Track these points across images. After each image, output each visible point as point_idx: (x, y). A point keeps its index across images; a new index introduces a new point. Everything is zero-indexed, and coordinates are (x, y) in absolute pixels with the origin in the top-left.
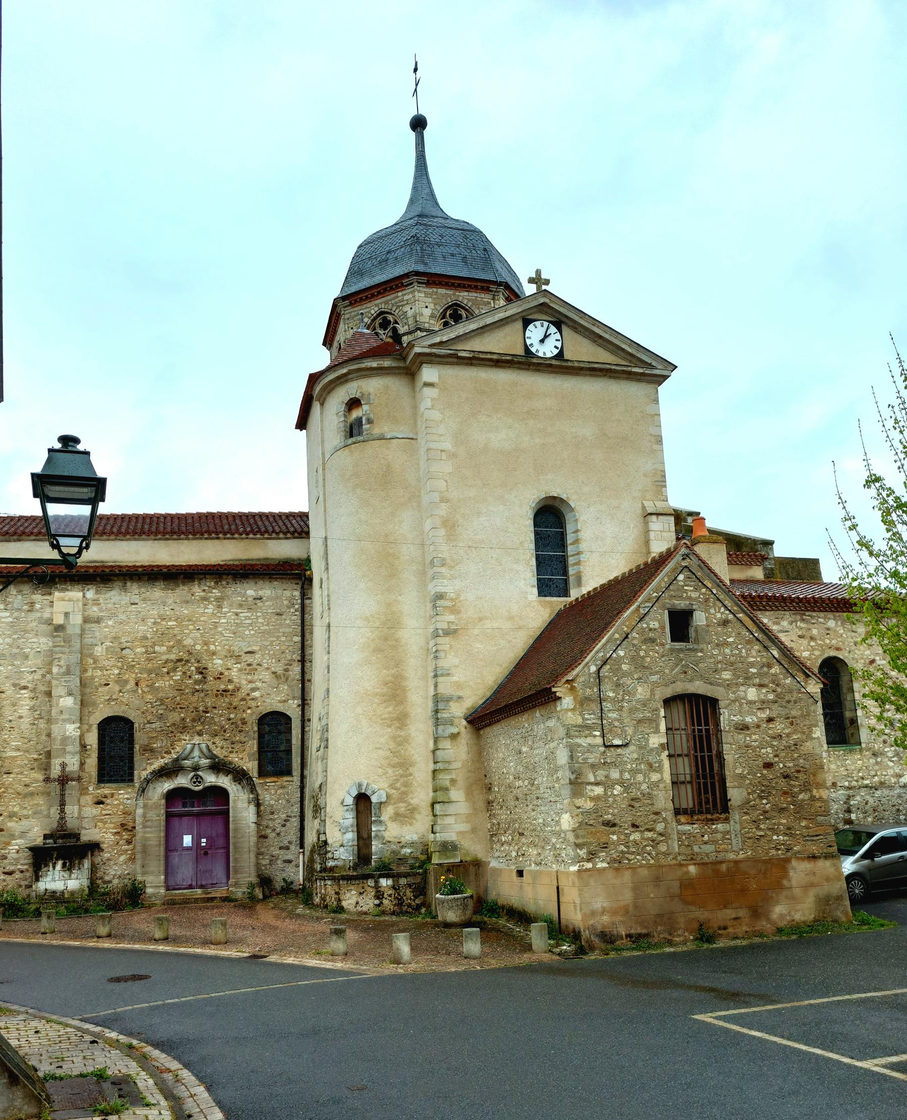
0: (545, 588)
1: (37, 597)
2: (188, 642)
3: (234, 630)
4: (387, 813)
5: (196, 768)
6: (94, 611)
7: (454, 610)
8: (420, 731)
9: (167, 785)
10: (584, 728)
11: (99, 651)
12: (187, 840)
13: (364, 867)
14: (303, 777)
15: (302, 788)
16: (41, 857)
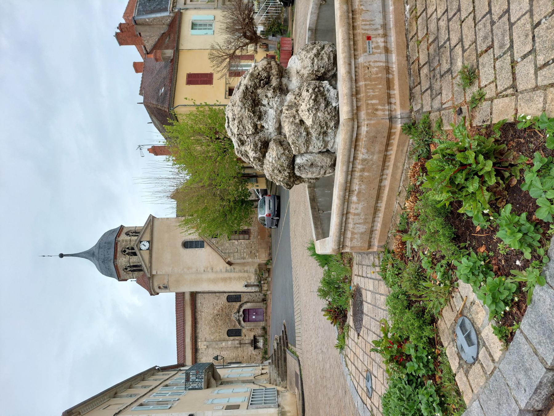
0: (202, 246)
1: (200, 352)
3: (207, 309)
4: (249, 281)
5: (239, 316)
6: (203, 339)
7: (207, 268)
8: (232, 275)
9: (242, 322)
11: (212, 338)
12: (254, 317)
13: (259, 286)
16: (256, 347)
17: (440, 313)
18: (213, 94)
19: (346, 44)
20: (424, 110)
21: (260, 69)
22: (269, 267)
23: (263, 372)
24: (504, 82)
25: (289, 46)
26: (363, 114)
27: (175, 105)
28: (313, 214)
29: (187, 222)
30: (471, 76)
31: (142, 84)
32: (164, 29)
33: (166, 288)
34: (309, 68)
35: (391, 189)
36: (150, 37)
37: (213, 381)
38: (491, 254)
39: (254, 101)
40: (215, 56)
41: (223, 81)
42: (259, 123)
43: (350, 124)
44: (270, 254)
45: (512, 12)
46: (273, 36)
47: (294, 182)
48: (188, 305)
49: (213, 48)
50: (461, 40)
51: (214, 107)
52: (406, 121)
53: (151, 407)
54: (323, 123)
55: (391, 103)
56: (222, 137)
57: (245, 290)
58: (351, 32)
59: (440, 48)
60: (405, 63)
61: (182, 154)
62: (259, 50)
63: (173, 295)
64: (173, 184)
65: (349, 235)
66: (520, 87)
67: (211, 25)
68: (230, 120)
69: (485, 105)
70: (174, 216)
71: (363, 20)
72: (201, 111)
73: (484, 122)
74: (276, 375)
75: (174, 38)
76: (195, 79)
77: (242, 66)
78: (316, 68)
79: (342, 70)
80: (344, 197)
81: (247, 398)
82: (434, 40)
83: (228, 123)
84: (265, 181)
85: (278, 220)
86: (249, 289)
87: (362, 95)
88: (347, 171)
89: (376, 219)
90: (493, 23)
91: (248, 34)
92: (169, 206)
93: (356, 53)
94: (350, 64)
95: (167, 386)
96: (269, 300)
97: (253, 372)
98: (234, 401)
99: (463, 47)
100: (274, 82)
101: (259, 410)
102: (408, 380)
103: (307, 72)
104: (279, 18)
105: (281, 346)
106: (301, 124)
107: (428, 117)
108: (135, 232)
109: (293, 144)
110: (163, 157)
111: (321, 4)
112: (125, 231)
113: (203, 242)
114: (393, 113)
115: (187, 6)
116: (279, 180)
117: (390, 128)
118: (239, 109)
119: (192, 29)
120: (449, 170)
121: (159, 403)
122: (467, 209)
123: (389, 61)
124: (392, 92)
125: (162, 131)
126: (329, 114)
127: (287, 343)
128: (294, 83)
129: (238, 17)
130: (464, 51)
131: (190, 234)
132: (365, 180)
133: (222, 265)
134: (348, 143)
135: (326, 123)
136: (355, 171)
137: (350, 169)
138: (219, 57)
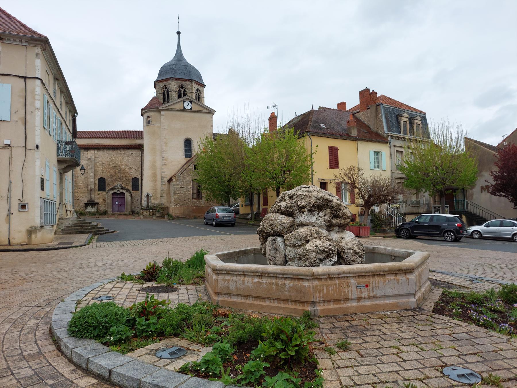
0: (186, 156)
2: (117, 162)
3: (126, 160)
4: (152, 198)
5: (118, 189)
6: (97, 156)
7: (166, 160)
8: (159, 183)
9: (112, 192)
10: (177, 184)
11: (98, 164)
12: (117, 203)
13: (148, 208)
14: (141, 191)
15: (141, 193)
16: (87, 205)
17: (183, 338)
18: (321, 169)
19: (363, 270)
20: (321, 325)
21: (344, 211)
22: (166, 217)
23: (68, 212)
24: (341, 363)
25: (363, 234)
26: (316, 283)
27: (311, 137)
28: (234, 252)
29: (209, 143)
30: (344, 347)
31: (328, 109)
32: (373, 128)
33: (148, 123)
34: (346, 247)
35: (263, 307)
36: (367, 117)
37: (64, 166)
38: (233, 362)
39: (322, 206)
40: (353, 172)
41: (333, 178)
42: (306, 210)
43: (310, 274)
44: (178, 218)
45: (383, 365)
46: (371, 220)
47: (263, 236)
48: (131, 142)
49: (359, 169)
50: (366, 342)
51: (310, 169)
52: (313, 314)
53: (46, 111)
54: (307, 257)
55: (324, 302)
56: (286, 176)
57: (144, 195)
58: (370, 274)
59: (362, 332)
60: (352, 311)
61: (271, 142)
62: (359, 208)
63: (141, 129)
64: (244, 133)
65: (227, 277)
66: (338, 370)
67: (378, 167)
68: (308, 189)
69: (327, 355)
70: (215, 131)
71: (378, 282)
72: (307, 158)
73: (316, 355)
74: (67, 224)
75: (367, 137)
76: (333, 153)
77: (345, 193)
78: (346, 251)
79: (345, 268)
80: (257, 272)
81: (49, 197)
82: (367, 329)
83: (305, 188)
84: (247, 213)
85: (212, 225)
86: (144, 198)
87: (329, 282)
88: (276, 273)
89: (240, 297)
90: (376, 357)
91: (372, 199)
92: (225, 129)
93: (357, 277)
94: (349, 273)
95: (61, 124)
96: (134, 217)
97: (69, 202)
98: (47, 184)
99: (362, 343)
100: (335, 221)
101: (39, 209)
102: (129, 320)
103: (343, 245)
104: (386, 225)
105: (94, 228)
106: (306, 241)
107: (316, 327)
108: (199, 97)
109: (292, 235)
110: (267, 125)
111: (392, 256)
112: (201, 88)
113: (190, 157)
114: (318, 304)
115: (392, 147)
116: (264, 224)
117: (307, 303)
118: (316, 196)
119: (375, 152)
120: (288, 330)
121: (49, 118)
122: (262, 345)
123: (352, 301)
124: (332, 303)
125: (290, 124)
126: (314, 261)
127: (98, 234)
128: (335, 236)
129: (385, 190)
130: (360, 344)
131: (199, 146)
132: (270, 287)
133: (168, 173)
134: (296, 273)
135: (308, 259)
136: (277, 279)
137: (278, 276)
138: (352, 175)
